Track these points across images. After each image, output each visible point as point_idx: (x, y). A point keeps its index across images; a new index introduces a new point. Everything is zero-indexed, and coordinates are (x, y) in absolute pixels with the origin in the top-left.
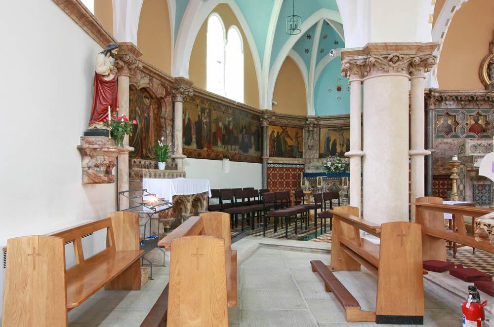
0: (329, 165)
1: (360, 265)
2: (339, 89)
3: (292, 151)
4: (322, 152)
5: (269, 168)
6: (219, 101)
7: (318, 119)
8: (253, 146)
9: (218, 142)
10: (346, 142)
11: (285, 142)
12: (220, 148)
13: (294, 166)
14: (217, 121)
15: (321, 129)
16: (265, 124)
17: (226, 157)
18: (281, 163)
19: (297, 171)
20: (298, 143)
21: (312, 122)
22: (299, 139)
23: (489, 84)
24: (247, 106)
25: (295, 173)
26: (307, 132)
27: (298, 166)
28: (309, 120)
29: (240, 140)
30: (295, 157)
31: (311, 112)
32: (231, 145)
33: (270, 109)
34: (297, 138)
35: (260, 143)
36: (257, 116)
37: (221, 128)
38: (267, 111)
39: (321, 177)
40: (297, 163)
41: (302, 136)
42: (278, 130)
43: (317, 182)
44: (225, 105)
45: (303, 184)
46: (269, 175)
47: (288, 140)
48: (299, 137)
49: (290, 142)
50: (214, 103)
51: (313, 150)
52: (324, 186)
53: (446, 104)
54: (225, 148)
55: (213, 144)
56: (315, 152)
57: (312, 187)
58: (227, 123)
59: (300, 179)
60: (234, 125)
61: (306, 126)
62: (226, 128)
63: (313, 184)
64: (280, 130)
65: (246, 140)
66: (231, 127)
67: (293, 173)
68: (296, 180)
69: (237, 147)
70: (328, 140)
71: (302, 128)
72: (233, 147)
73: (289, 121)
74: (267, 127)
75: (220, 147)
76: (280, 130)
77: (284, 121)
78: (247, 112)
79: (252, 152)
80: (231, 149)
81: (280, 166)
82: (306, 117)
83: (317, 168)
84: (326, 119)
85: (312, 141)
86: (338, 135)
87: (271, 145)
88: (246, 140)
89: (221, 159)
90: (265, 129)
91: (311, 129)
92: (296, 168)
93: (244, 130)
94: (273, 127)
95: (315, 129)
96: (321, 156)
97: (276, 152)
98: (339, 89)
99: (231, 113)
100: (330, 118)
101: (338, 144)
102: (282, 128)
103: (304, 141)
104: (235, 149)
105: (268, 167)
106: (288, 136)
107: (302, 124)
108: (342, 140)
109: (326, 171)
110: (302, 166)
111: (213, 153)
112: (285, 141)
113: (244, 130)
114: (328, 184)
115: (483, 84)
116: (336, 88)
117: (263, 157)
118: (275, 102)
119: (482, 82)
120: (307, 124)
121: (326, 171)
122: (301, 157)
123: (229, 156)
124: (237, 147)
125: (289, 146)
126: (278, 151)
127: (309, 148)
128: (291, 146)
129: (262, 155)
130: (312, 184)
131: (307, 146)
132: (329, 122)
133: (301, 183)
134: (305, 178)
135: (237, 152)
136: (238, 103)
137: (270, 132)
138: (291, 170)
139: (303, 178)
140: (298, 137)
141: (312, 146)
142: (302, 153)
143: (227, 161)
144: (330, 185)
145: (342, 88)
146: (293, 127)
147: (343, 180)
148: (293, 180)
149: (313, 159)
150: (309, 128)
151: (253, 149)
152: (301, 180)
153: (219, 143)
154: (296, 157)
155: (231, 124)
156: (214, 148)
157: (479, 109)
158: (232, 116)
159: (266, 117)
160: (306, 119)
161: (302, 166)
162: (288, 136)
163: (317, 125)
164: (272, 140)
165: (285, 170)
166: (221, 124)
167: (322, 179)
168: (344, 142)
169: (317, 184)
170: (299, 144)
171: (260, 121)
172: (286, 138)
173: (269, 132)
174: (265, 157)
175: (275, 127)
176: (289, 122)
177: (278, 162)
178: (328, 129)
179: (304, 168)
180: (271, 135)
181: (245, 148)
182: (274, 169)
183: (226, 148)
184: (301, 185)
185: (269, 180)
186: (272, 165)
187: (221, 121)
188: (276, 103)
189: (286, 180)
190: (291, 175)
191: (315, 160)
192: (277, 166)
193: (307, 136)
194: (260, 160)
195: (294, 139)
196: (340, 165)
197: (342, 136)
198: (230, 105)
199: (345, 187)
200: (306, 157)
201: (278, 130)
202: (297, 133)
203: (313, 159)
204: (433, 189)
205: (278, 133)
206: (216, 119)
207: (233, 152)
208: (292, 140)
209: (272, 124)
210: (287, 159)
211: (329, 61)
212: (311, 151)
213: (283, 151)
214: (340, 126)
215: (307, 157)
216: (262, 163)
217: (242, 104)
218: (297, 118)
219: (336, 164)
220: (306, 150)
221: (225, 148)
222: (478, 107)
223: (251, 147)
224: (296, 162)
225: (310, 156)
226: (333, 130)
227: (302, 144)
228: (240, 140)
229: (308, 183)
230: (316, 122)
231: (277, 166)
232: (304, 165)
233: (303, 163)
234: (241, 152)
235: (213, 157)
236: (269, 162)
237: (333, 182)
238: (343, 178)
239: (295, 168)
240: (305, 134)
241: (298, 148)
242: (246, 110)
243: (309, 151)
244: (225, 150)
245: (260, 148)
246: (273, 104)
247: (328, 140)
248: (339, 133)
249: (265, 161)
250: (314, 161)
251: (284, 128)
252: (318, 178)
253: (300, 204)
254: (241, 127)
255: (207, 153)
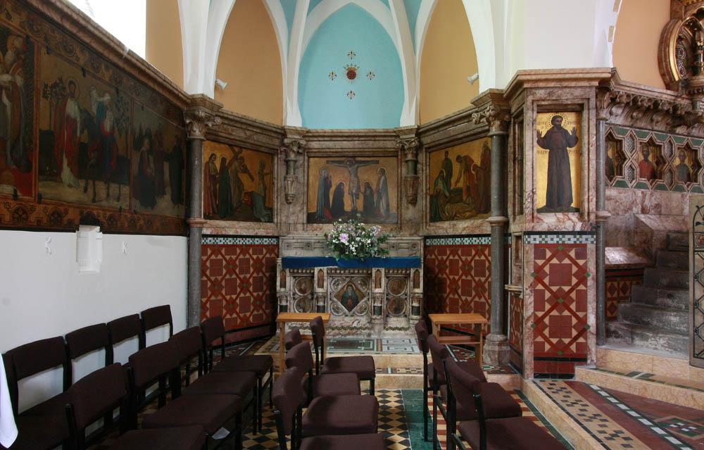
0: (345, 241)
1: (307, 407)
2: (351, 74)
3: (252, 205)
4: (313, 210)
5: (204, 247)
6: (67, 25)
7: (307, 135)
8: (168, 190)
9: (60, 169)
10: (362, 189)
11: (239, 184)
12: (69, 189)
13: (257, 242)
14: (60, 91)
15: (311, 159)
16: (197, 132)
17: (90, 221)
18: (231, 233)
19: (265, 251)
20: (265, 189)
21: (294, 142)
22: (267, 178)
23: (677, 79)
24: (149, 67)
25: (261, 256)
26: (283, 162)
27: (266, 241)
28: (289, 136)
29: (135, 168)
30: (258, 220)
31: (293, 119)
32: (107, 182)
33: (211, 95)
34: (262, 175)
35: (184, 183)
36: (179, 108)
37: (75, 120)
38: (203, 99)
39: (325, 269)
40: (264, 234)
41: (272, 172)
42: (222, 153)
43: (316, 279)
44: (86, 47)
45: (283, 285)
46: (207, 272)
47: (244, 178)
48: (267, 174)
49: (248, 185)
50: (47, 26)
51: (295, 205)
52: (329, 290)
53: (611, 114)
54: (86, 190)
55: (41, 172)
56: (299, 208)
57: (301, 290)
58: (94, 110)
59: (585, 310)
60: (117, 121)
61: (283, 149)
62: (91, 123)
63: (306, 286)
64: (228, 155)
65: (150, 170)
66: (108, 125)
67: (255, 257)
68: (261, 275)
69: (126, 190)
70: (326, 184)
71: (272, 153)
72: (114, 188)
73: (248, 133)
74: (202, 140)
75: (70, 186)
76: (228, 155)
77: (239, 134)
78: (154, 90)
79: (165, 206)
80: (108, 195)
81: (230, 241)
82: (283, 128)
83: (308, 246)
84: (324, 136)
85: (294, 184)
86: (347, 174)
87: (207, 189)
88: (150, 170)
89: (71, 227)
90: (196, 144)
91: (292, 156)
92: (234, 246)
93: (146, 141)
94: (213, 144)
95: (301, 158)
96: (312, 219)
97: (217, 206)
98: (351, 74)
99: (107, 79)
100: (334, 136)
101: (346, 194)
102: (234, 151)
103: (279, 183)
104: (119, 196)
105: (203, 245)
106: (246, 171)
107: (269, 147)
108: (356, 185)
109: (335, 255)
110: (274, 241)
111: (39, 208)
112: (238, 181)
113: (146, 141)
114: (336, 284)
115: (663, 79)
116: (347, 72)
117: (192, 220)
118: (219, 82)
119: (663, 75)
120: (283, 145)
121: (335, 255)
122: (271, 221)
123: (101, 218)
124: (126, 190)
125: (246, 193)
126: (222, 208)
127: (287, 200)
128: (250, 194)
129: (188, 213)
130: (299, 284)
131: (283, 194)
132: (330, 144)
133: (278, 283)
134: (287, 271)
135: (125, 204)
136: (130, 53)
137: (206, 155)
138: (223, 251)
139: (283, 270)
140: (266, 174)
141: (294, 196)
142: (271, 210)
143: (92, 235)
144: (340, 287)
145: (357, 72)
146: (256, 149)
147: (374, 275)
148: (255, 275)
149: (295, 224)
150: (287, 156)
151: (168, 197)
152: (278, 274)
153: (66, 173)
154: (261, 221)
155: (109, 114)
156: (46, 189)
157: (653, 130)
158: (113, 91)
159: (202, 114)
160: (282, 133)
161: (274, 241)
162: (246, 171)
163: (305, 149)
164: (211, 177)
165: (238, 251)
166: (72, 109)
167: (325, 274)
168: (359, 188)
169: (316, 285)
170: (268, 188)
171: (184, 124)
172: (240, 175)
173: (205, 158)
174: (198, 220)
175: (217, 145)
176: (249, 137)
177: (224, 233)
178: (325, 160)
179: (278, 245)
180: (207, 163)
181: (147, 194)
182: (216, 249)
183: (90, 191)
184: (278, 288)
185: (205, 278)
186: (210, 241)
187: (72, 96)
188: (223, 85)
189: (242, 276)
190: (252, 262)
191: (300, 227)
192: (221, 241)
193: (284, 173)
194: (182, 228)
195: (257, 178)
196: (369, 241)
197: (356, 176)
198: (106, 53)
199: (377, 290)
200: (281, 220)
201: (222, 153)
202: (263, 166)
203: (295, 224)
204: (609, 299)
205: (223, 160)
206: (55, 85)
207: (115, 204)
208: (253, 179)
209: (212, 136)
210: (242, 224)
211: (327, 16)
212: (291, 206)
213: (235, 205)
214: (351, 154)
215: (284, 219)
216: (188, 236)
217: (139, 59)
218: (265, 129)
219: (358, 239)
220: (282, 204)
221: (86, 190)
222: (651, 126)
223: (164, 193)
224: (262, 232)
225: (287, 217)
226: (337, 162)
227: (271, 189)
228: (135, 168)
229: (293, 280)
230: (303, 142)
231: (221, 241)
232: (277, 238)
233: (276, 235)
234: (136, 204)
235: (39, 221)
236: (206, 231)
237: (348, 279)
238: (374, 270)
239: (233, 245)
240: (279, 169)
241: (264, 198)
242: (151, 84)
243: (287, 205)
244: (86, 198)
245: (183, 197)
246: (217, 87)
247: (326, 184)
248: (350, 169)
249: (195, 230)
250: (296, 230)
251: (237, 149)
252: (317, 269)
253: (479, 398)
254: (137, 131)
255: (14, 205)
